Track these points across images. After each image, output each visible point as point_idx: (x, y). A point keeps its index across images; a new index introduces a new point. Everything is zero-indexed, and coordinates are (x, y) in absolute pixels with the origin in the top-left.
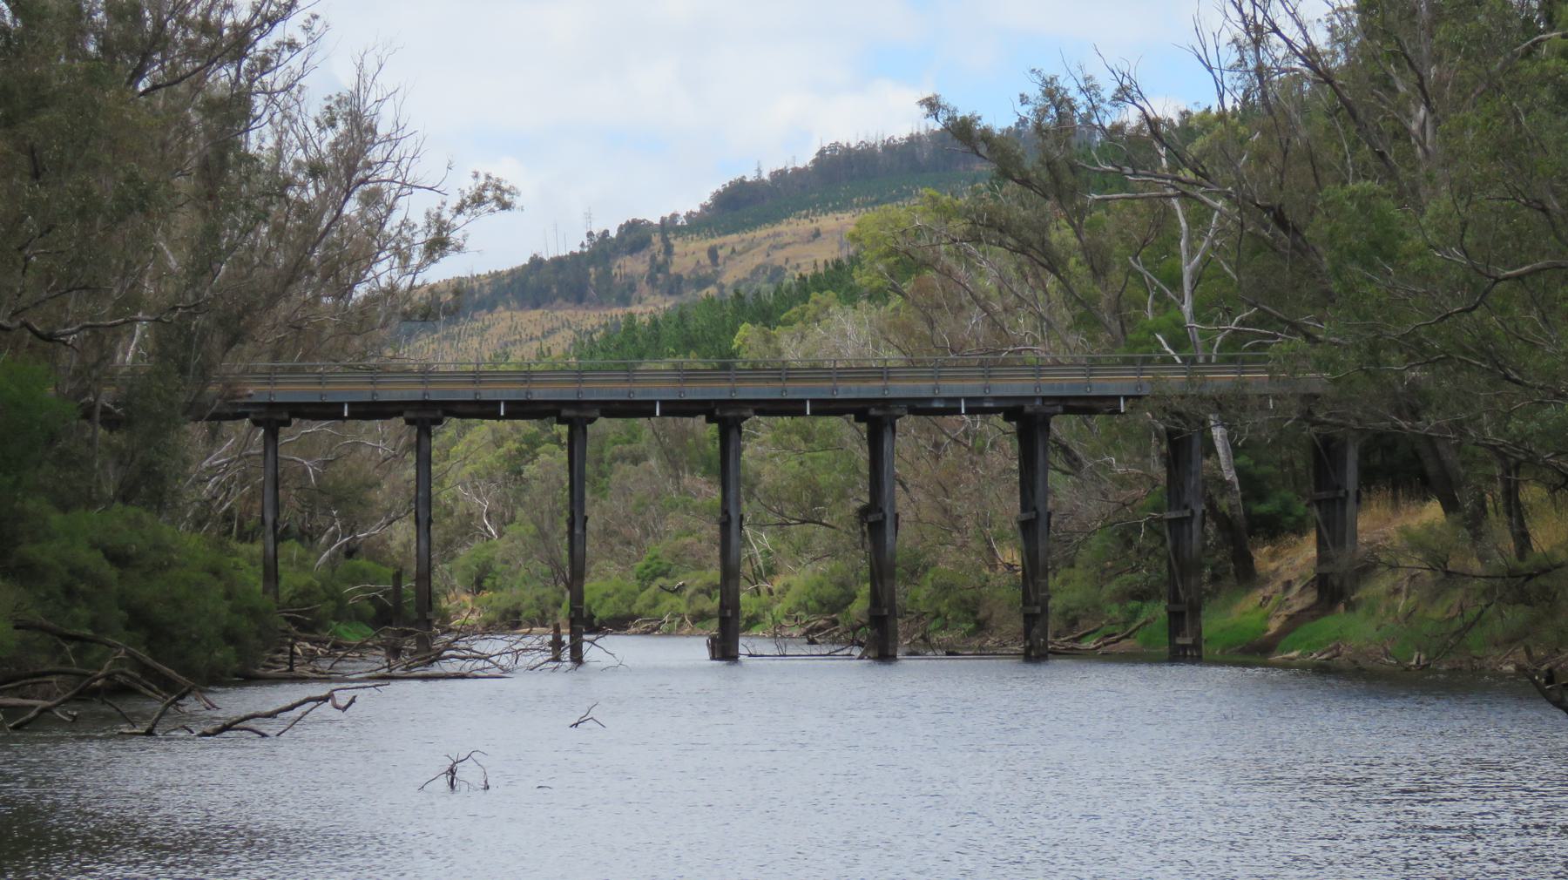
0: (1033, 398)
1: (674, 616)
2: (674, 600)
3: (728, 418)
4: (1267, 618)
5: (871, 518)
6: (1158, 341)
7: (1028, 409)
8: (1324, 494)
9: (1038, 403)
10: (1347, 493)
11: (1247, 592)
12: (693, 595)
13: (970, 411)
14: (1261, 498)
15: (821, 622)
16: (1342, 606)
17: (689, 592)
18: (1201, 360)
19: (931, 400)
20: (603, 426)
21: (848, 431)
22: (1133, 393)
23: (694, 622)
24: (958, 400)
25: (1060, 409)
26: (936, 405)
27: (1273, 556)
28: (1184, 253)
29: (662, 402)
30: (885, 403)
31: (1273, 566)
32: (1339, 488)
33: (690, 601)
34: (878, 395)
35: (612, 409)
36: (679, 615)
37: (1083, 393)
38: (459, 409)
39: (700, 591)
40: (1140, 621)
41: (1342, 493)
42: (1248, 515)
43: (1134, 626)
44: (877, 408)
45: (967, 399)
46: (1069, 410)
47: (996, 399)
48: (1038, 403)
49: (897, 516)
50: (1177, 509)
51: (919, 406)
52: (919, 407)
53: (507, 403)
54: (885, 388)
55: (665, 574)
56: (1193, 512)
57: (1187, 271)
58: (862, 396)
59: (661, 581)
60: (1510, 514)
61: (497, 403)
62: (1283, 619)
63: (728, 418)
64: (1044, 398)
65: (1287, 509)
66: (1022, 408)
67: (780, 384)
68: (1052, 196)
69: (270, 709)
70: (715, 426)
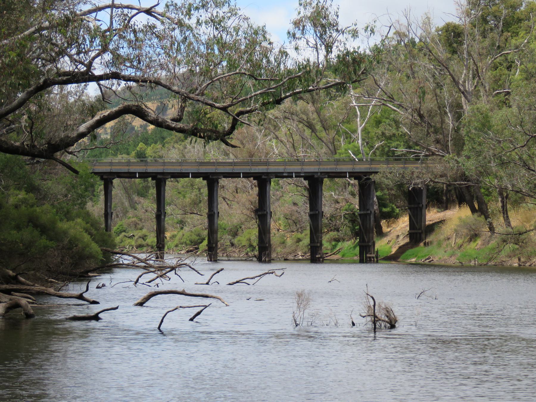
0: (317, 173)
1: (130, 246)
2: (129, 240)
3: (160, 179)
4: (391, 247)
5: (260, 213)
6: (349, 153)
7: (316, 176)
8: (413, 206)
9: (319, 174)
10: (423, 205)
11: (381, 239)
12: (137, 239)
13: (296, 177)
14: (385, 206)
15: (191, 249)
16: (422, 244)
17: (136, 237)
18: (364, 160)
19: (283, 173)
20: (223, 182)
21: (200, 182)
22: (351, 171)
23: (137, 248)
24: (292, 173)
25: (327, 176)
26: (285, 175)
27: (388, 226)
28: (359, 123)
29: (243, 173)
30: (267, 174)
31: (389, 229)
32: (419, 204)
33: (136, 241)
34: (265, 171)
35: (119, 175)
36: (131, 246)
37: (334, 171)
38: (122, 175)
39: (140, 237)
40: (337, 248)
41: (421, 205)
42: (381, 211)
43: (335, 251)
44: (265, 176)
45: (295, 173)
46: (172, 177)
47: (305, 173)
48: (319, 174)
49: (218, 213)
50: (364, 210)
51: (279, 175)
52: (333, 175)
53: (139, 173)
54: (336, 168)
55: (124, 231)
56: (371, 212)
57: (360, 129)
58: (261, 171)
59: (123, 234)
60: (504, 214)
61: (136, 173)
62: (397, 248)
63: (160, 179)
64: (321, 173)
65: (393, 210)
66: (314, 176)
67: (266, 167)
68: (311, 103)
69: (193, 267)
70: (155, 181)
